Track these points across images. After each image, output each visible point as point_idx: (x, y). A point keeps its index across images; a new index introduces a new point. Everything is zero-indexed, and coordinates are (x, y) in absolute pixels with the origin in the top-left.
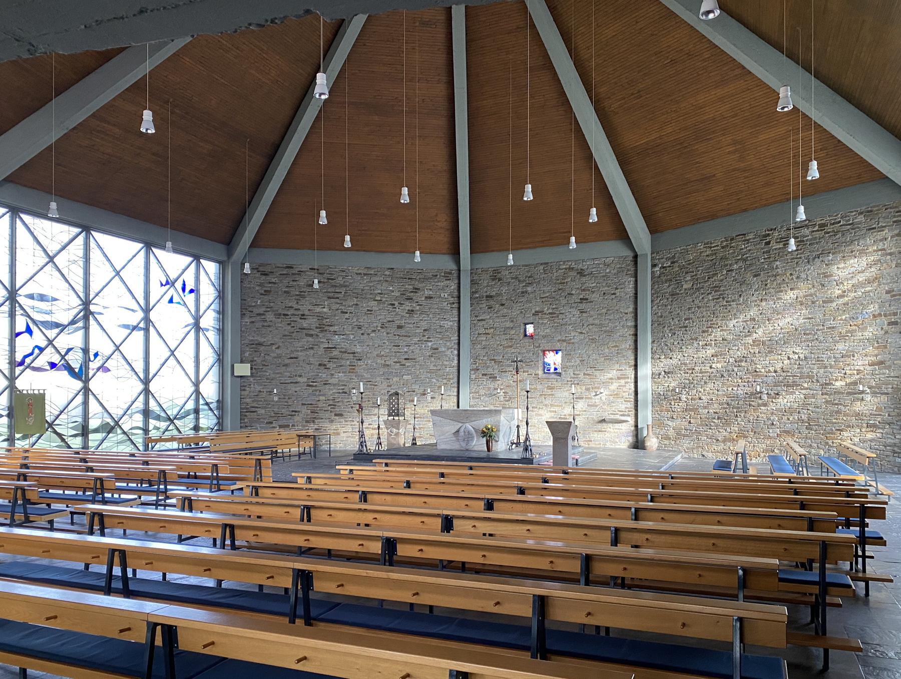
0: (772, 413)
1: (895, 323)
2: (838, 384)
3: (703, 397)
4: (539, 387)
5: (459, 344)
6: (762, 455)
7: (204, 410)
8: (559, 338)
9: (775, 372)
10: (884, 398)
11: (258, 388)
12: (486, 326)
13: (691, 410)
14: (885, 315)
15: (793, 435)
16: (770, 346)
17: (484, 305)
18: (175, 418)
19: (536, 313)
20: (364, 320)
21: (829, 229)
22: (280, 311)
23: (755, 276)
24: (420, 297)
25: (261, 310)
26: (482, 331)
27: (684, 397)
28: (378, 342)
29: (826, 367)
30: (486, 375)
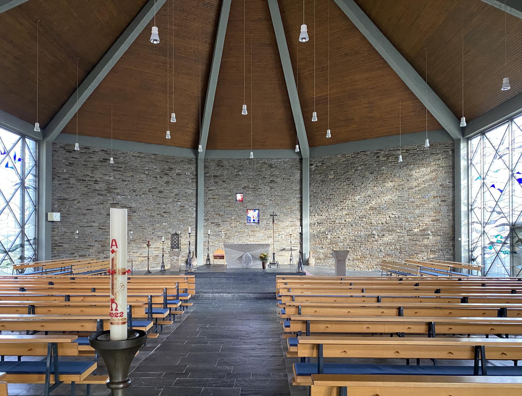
0: (380, 245)
1: (444, 201)
2: (416, 230)
3: (341, 237)
4: (246, 230)
5: (197, 204)
6: (375, 267)
7: (27, 245)
8: (258, 202)
9: (382, 224)
10: (439, 238)
11: (64, 230)
12: (213, 194)
13: (333, 243)
14: (440, 197)
15: (392, 257)
16: (378, 210)
17: (212, 181)
18: (9, 251)
19: (244, 188)
20: (137, 186)
21: (411, 152)
22: (79, 178)
23: (371, 174)
24: (173, 174)
25: (67, 176)
26: (211, 196)
27: (329, 237)
28: (146, 201)
29: (409, 222)
30: (213, 223)
